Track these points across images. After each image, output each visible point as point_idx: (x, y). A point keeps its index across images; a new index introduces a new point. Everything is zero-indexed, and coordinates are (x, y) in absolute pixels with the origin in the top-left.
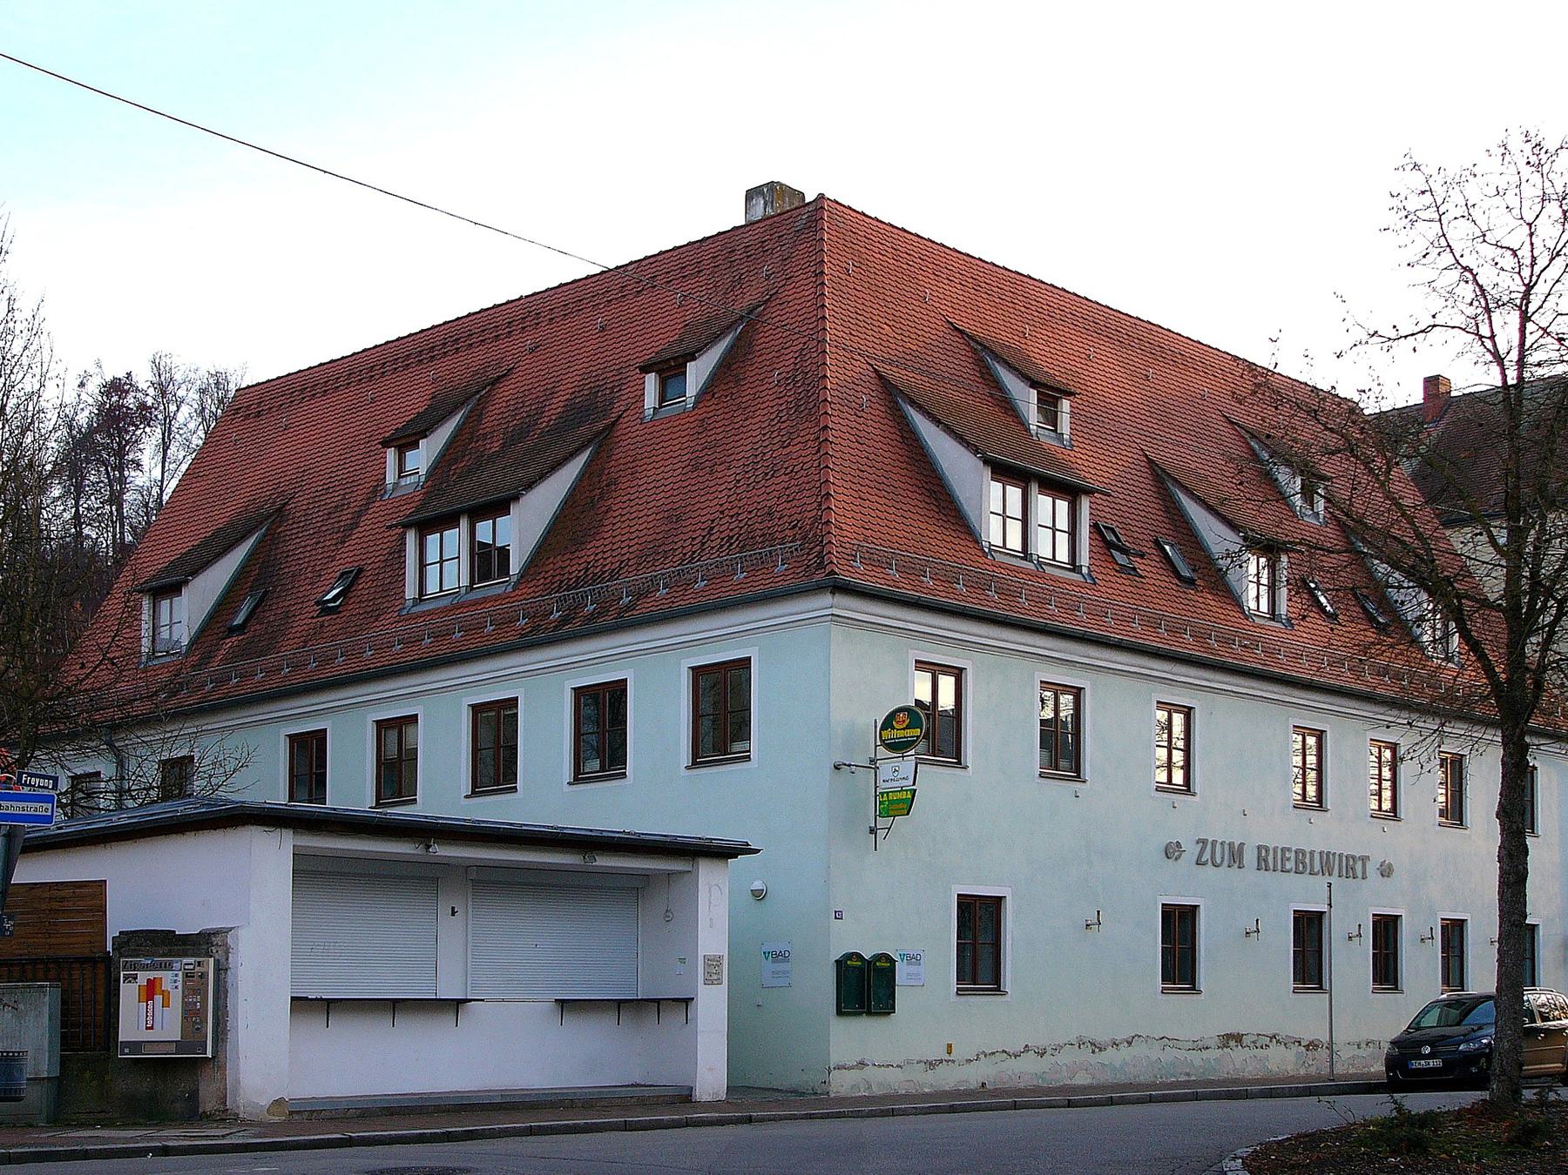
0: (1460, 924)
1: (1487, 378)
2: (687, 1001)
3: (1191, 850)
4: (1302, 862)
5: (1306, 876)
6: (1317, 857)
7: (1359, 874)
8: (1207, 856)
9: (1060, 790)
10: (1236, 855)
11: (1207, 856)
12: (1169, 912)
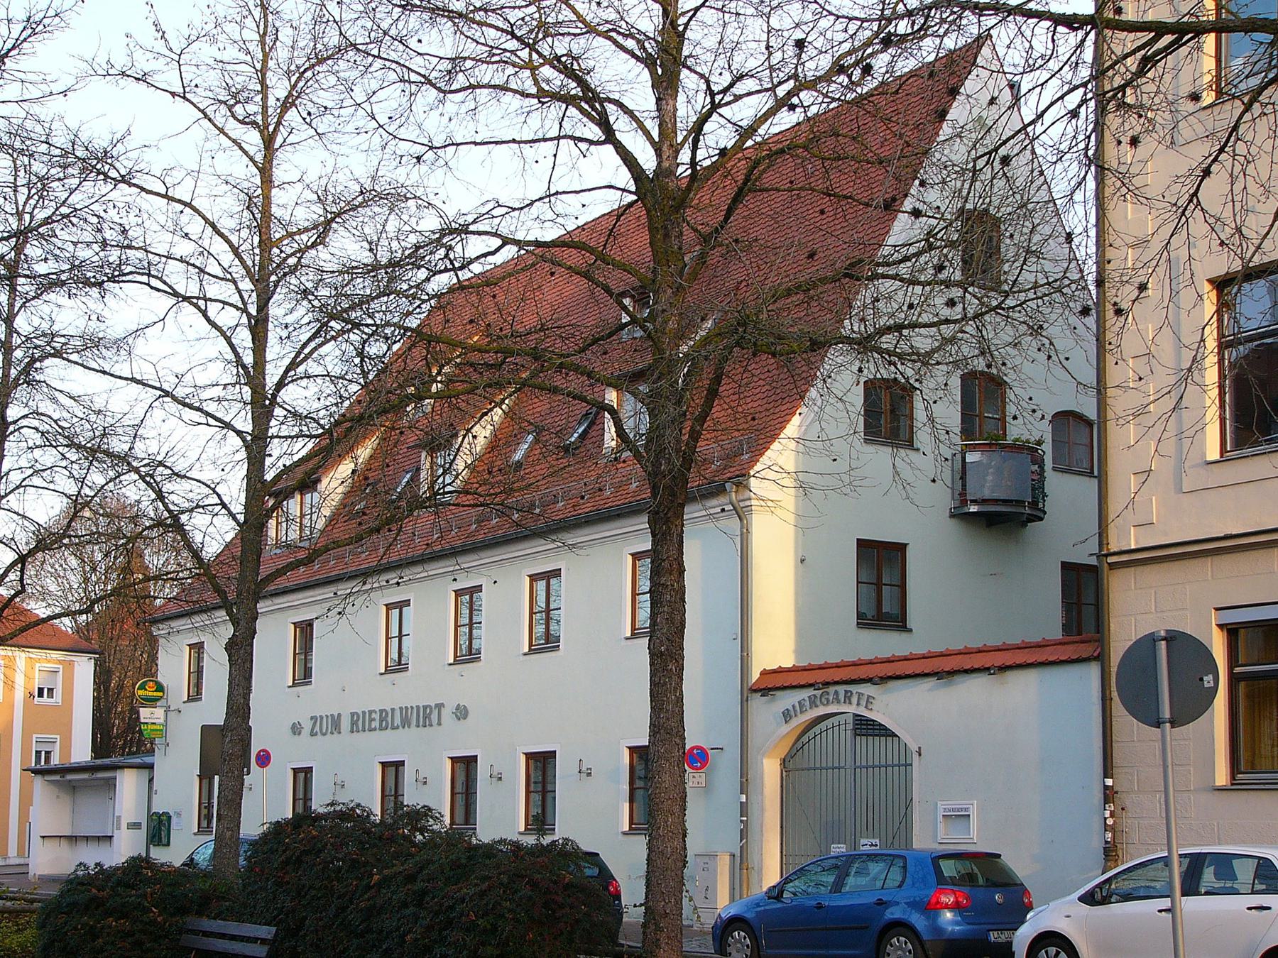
0: (308, 771)
1: (591, 185)
2: (111, 837)
3: (307, 725)
4: (385, 720)
5: (421, 729)
6: (397, 713)
7: (435, 721)
8: (317, 729)
9: (881, 456)
10: (336, 722)
11: (317, 729)
12: (296, 771)
